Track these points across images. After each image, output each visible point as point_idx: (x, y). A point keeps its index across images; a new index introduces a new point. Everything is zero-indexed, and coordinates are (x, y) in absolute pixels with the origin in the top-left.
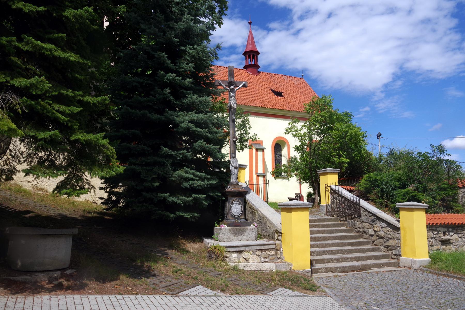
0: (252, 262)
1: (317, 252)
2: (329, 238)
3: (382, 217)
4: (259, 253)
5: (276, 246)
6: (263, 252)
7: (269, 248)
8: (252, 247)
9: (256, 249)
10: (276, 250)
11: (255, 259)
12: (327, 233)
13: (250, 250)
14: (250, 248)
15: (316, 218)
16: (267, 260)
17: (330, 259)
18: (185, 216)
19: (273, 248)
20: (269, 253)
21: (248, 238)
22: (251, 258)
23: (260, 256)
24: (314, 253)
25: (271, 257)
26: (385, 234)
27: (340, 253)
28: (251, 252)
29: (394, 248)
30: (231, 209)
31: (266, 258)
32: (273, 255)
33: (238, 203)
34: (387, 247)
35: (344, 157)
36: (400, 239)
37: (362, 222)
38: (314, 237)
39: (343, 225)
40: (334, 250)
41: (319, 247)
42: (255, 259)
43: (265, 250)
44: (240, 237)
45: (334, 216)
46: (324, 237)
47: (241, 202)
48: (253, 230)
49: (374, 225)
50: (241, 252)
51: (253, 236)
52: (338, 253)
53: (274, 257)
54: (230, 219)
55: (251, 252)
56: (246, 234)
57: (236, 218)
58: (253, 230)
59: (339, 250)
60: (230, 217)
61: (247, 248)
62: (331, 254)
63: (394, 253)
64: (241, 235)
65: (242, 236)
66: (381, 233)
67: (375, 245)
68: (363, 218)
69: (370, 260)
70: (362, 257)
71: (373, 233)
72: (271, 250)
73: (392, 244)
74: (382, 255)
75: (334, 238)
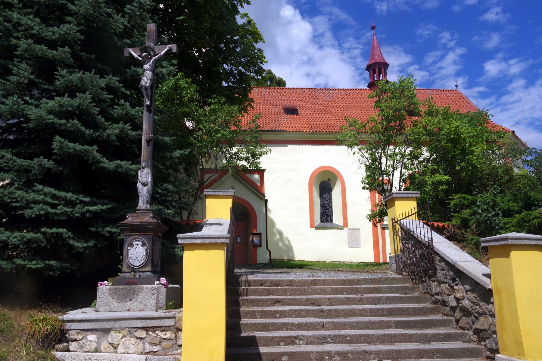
0: (123, 351)
1: (308, 337)
2: (362, 313)
3: (464, 268)
4: (143, 334)
5: (176, 323)
6: (150, 333)
7: (161, 325)
8: (129, 322)
9: (135, 326)
10: (175, 330)
11: (132, 346)
12: (367, 304)
13: (123, 329)
14: (124, 324)
15: (360, 277)
16: (155, 349)
17: (325, 352)
18: (28, 266)
19: (170, 324)
20: (162, 335)
21: (142, 306)
22: (121, 343)
23: (144, 341)
24: (301, 339)
25: (165, 344)
26: (472, 305)
27: (364, 342)
28: (125, 332)
29: (487, 336)
31: (156, 345)
32: (170, 339)
33: (140, 243)
34: (477, 332)
35: (442, 173)
36: (493, 316)
37: (440, 283)
38: (326, 310)
39: (412, 289)
40: (349, 336)
41: (328, 329)
42: (132, 346)
43: (154, 329)
44: (128, 304)
45: (404, 273)
46: (350, 310)
47: (146, 241)
48: (154, 292)
49: (455, 287)
50: (107, 331)
51: (151, 302)
52: (357, 342)
53: (171, 343)
54: (125, 272)
55: (125, 332)
56: (140, 297)
57: (134, 270)
58: (154, 292)
59: (360, 336)
60: (125, 269)
61: (117, 325)
62: (340, 343)
63: (489, 346)
64: (131, 300)
65: (131, 302)
66: (466, 303)
67: (462, 328)
68: (440, 274)
69: (427, 358)
70: (406, 351)
71: (454, 304)
72: (166, 328)
73: (483, 325)
74: (461, 349)
75: (374, 313)
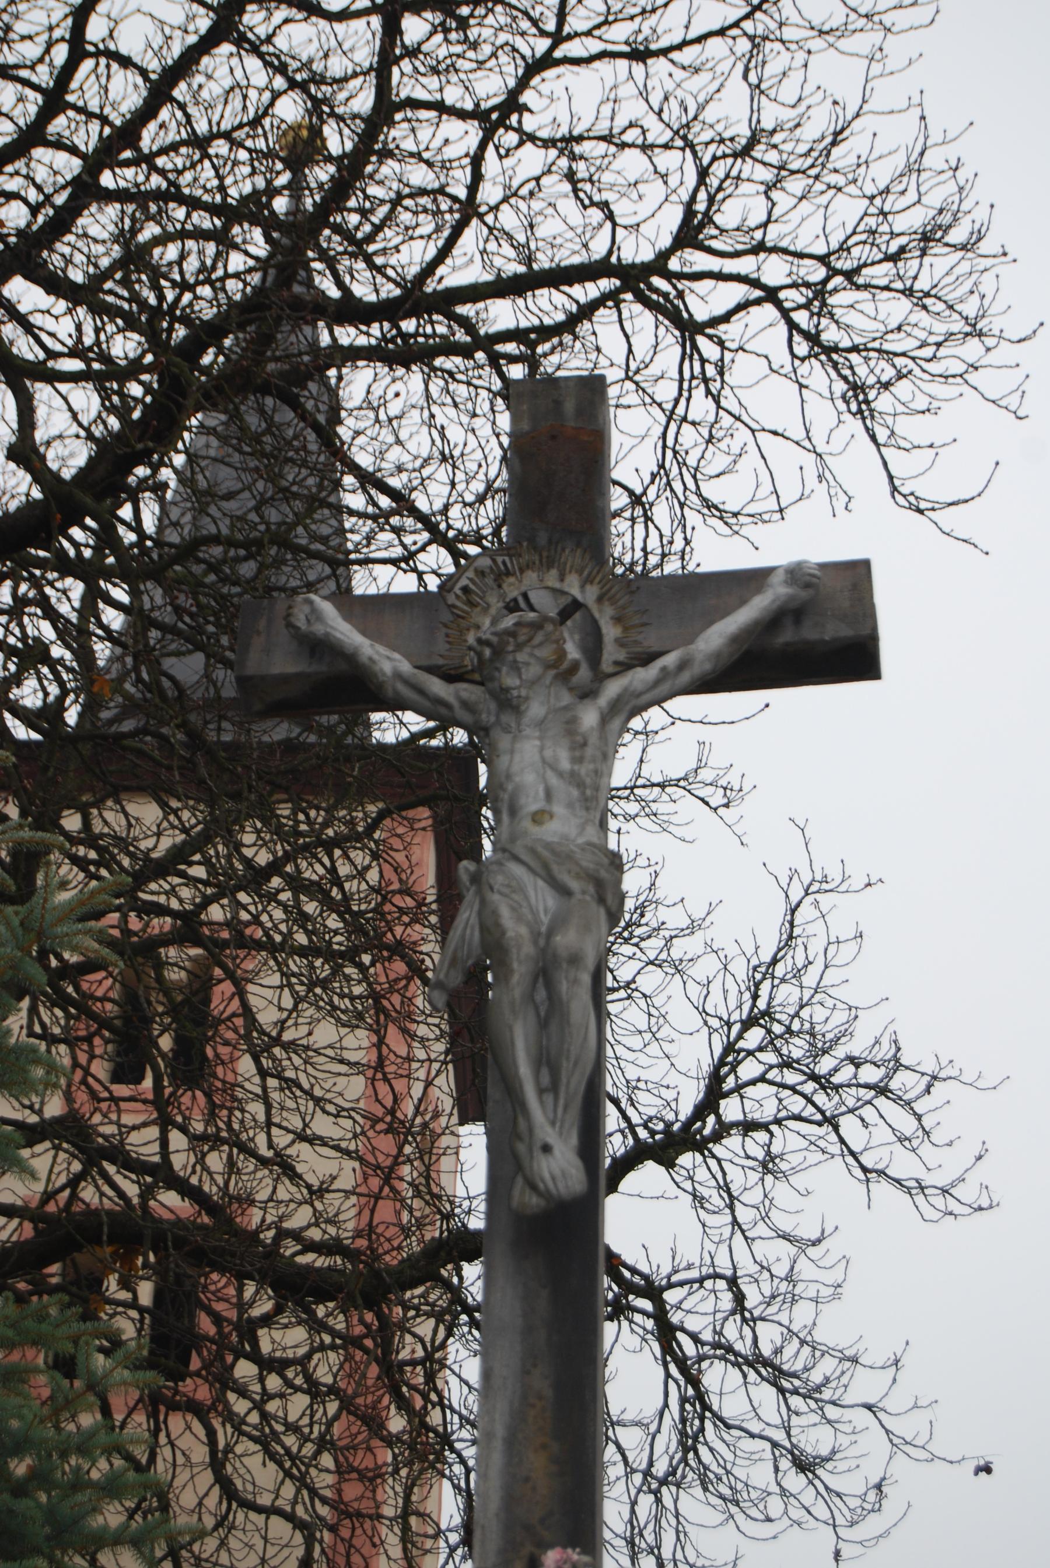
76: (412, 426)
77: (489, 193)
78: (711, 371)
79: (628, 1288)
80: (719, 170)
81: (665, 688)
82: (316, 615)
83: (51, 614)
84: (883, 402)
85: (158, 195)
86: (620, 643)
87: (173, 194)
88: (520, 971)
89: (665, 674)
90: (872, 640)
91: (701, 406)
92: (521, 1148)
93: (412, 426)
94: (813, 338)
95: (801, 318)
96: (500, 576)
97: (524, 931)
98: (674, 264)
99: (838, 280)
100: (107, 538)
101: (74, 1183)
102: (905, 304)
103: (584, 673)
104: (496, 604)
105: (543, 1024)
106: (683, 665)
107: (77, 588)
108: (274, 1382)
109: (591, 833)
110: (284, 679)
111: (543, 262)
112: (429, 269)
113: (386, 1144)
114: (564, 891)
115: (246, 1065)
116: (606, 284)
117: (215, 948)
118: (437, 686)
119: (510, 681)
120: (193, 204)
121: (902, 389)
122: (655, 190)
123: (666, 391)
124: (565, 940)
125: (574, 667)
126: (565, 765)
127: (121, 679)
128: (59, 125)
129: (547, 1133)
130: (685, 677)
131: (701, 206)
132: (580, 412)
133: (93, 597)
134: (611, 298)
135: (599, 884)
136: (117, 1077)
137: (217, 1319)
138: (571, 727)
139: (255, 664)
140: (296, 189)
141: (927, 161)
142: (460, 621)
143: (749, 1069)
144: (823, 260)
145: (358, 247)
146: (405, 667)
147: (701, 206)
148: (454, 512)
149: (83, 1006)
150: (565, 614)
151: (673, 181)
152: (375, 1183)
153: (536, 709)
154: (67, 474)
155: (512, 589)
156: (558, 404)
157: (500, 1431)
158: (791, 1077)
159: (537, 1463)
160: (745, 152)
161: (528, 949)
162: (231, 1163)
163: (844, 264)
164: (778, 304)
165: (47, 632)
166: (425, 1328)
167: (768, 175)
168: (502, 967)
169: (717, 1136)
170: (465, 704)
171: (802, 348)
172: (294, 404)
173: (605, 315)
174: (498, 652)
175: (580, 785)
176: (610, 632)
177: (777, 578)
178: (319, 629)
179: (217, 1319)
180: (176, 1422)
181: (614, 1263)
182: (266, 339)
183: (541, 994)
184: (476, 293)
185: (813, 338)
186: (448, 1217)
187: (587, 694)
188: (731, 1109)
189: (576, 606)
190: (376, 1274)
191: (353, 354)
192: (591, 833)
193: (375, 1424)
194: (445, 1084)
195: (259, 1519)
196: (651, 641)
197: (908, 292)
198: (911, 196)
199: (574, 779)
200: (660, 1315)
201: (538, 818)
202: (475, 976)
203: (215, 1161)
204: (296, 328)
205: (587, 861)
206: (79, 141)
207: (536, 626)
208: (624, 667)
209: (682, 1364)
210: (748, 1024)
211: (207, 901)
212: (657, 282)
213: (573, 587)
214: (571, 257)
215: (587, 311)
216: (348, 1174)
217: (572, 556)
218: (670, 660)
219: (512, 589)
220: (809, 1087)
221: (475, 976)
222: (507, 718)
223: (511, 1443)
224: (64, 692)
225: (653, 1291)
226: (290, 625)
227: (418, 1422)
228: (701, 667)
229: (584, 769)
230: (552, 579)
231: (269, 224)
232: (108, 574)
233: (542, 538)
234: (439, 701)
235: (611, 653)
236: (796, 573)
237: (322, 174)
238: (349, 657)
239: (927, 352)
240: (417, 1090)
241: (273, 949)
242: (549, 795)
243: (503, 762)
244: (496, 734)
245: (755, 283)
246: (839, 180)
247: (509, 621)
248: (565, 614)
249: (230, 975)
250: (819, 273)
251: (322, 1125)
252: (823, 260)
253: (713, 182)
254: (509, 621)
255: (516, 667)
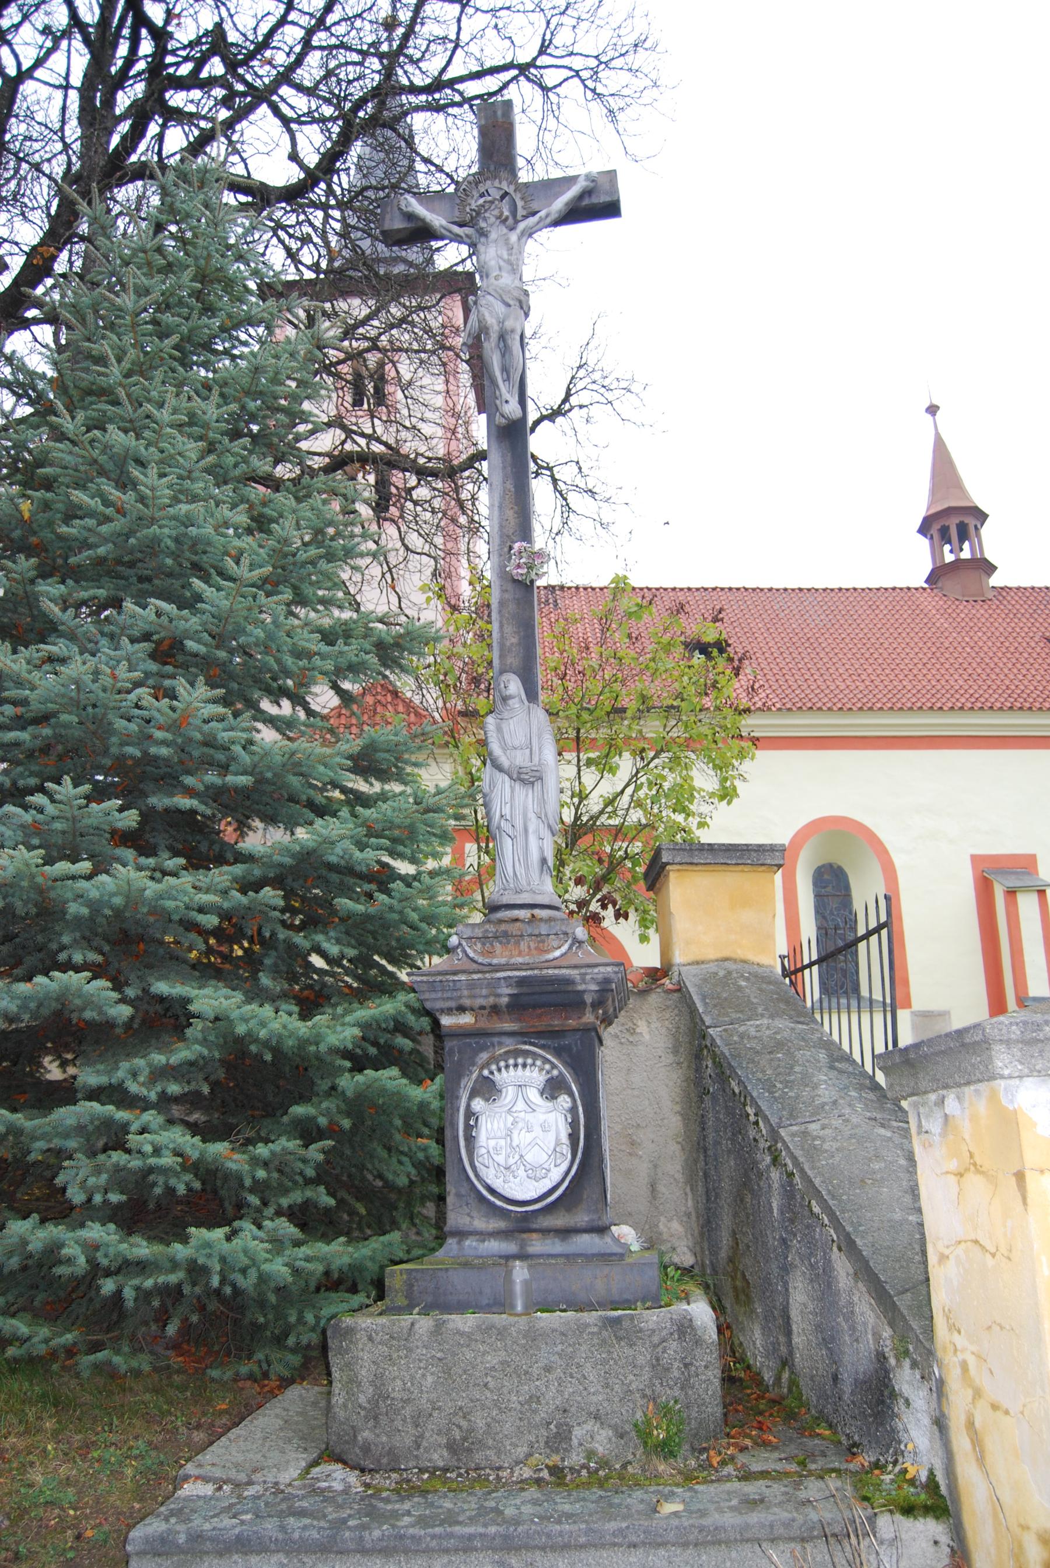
30: (470, 1140)
76: (442, 139)
77: (464, 37)
78: (555, 107)
79: (540, 467)
80: (554, 22)
81: (541, 225)
82: (408, 204)
83: (311, 224)
84: (620, 116)
85: (336, 47)
86: (524, 208)
87: (343, 46)
88: (494, 336)
89: (541, 220)
90: (618, 201)
91: (552, 123)
92: (498, 402)
93: (442, 139)
94: (594, 91)
95: (589, 83)
96: (477, 183)
97: (494, 321)
98: (538, 63)
99: (603, 66)
100: (330, 192)
101: (343, 443)
102: (629, 75)
103: (510, 221)
104: (476, 194)
105: (503, 355)
106: (547, 216)
107: (320, 214)
108: (419, 508)
109: (517, 283)
110: (399, 231)
111: (488, 65)
112: (444, 70)
113: (453, 421)
114: (508, 305)
115: (400, 395)
116: (514, 72)
117: (383, 351)
118: (456, 229)
119: (483, 224)
120: (350, 49)
121: (628, 111)
122: (529, 30)
123: (538, 117)
124: (509, 324)
125: (507, 219)
126: (506, 257)
127: (341, 250)
128: (293, 16)
129: (506, 395)
130: (549, 220)
131: (548, 37)
132: (503, 115)
133: (327, 216)
134: (515, 78)
135: (520, 302)
136: (354, 405)
137: (397, 488)
138: (507, 240)
139: (387, 226)
140: (389, 39)
141: (636, 13)
142: (463, 203)
143: (580, 385)
144: (596, 57)
145: (415, 62)
146: (444, 222)
147: (548, 37)
148: (460, 171)
149: (337, 376)
150: (503, 197)
151: (536, 25)
152: (449, 435)
153: (493, 236)
154: (312, 166)
155: (482, 189)
156: (495, 112)
157: (497, 504)
158: (594, 387)
159: (510, 514)
160: (563, 13)
161: (496, 328)
162: (398, 431)
163: (604, 59)
164: (580, 77)
165: (310, 230)
166: (470, 487)
167: (574, 22)
168: (488, 338)
169: (570, 410)
170: (467, 236)
171: (590, 95)
172: (395, 130)
173: (513, 87)
174: (478, 213)
175: (511, 264)
176: (520, 204)
177: (581, 179)
178: (410, 209)
179: (397, 488)
180: (387, 524)
181: (534, 458)
182: (382, 103)
183: (502, 344)
184: (461, 79)
185: (594, 91)
186: (475, 445)
187: (512, 229)
188: (574, 400)
189: (506, 194)
190: (452, 467)
191: (418, 109)
192: (517, 283)
193: (454, 520)
194: (471, 400)
195: (417, 557)
196: (535, 206)
197: (630, 70)
198: (629, 29)
199: (509, 262)
200: (552, 476)
201: (496, 278)
202: (478, 338)
203: (393, 429)
204: (394, 98)
205: (516, 294)
206: (301, 23)
207: (492, 202)
208: (525, 217)
209: (560, 493)
210: (580, 367)
211: (380, 334)
212: (532, 70)
213: (505, 186)
214: (499, 62)
215: (505, 85)
216: (440, 432)
217: (503, 174)
218: (542, 214)
219: (482, 189)
220: (603, 390)
221: (478, 338)
222: (483, 240)
223: (500, 507)
224: (320, 256)
225: (549, 468)
226: (400, 209)
227: (472, 521)
228: (554, 216)
229: (513, 258)
230: (496, 183)
231: (381, 56)
232: (332, 207)
233: (492, 168)
234: (457, 235)
235: (521, 212)
236: (588, 177)
237: (400, 31)
238: (423, 220)
239: (638, 95)
240: (462, 400)
241: (407, 351)
242: (500, 269)
243: (482, 257)
244: (479, 246)
245: (570, 69)
246: (601, 23)
247: (481, 201)
248: (503, 197)
249: (392, 361)
250: (595, 63)
251: (428, 415)
252: (596, 57)
253: (552, 26)
254: (481, 201)
255: (485, 219)
